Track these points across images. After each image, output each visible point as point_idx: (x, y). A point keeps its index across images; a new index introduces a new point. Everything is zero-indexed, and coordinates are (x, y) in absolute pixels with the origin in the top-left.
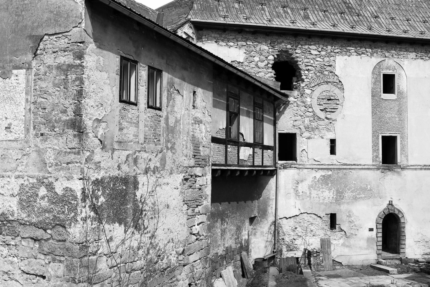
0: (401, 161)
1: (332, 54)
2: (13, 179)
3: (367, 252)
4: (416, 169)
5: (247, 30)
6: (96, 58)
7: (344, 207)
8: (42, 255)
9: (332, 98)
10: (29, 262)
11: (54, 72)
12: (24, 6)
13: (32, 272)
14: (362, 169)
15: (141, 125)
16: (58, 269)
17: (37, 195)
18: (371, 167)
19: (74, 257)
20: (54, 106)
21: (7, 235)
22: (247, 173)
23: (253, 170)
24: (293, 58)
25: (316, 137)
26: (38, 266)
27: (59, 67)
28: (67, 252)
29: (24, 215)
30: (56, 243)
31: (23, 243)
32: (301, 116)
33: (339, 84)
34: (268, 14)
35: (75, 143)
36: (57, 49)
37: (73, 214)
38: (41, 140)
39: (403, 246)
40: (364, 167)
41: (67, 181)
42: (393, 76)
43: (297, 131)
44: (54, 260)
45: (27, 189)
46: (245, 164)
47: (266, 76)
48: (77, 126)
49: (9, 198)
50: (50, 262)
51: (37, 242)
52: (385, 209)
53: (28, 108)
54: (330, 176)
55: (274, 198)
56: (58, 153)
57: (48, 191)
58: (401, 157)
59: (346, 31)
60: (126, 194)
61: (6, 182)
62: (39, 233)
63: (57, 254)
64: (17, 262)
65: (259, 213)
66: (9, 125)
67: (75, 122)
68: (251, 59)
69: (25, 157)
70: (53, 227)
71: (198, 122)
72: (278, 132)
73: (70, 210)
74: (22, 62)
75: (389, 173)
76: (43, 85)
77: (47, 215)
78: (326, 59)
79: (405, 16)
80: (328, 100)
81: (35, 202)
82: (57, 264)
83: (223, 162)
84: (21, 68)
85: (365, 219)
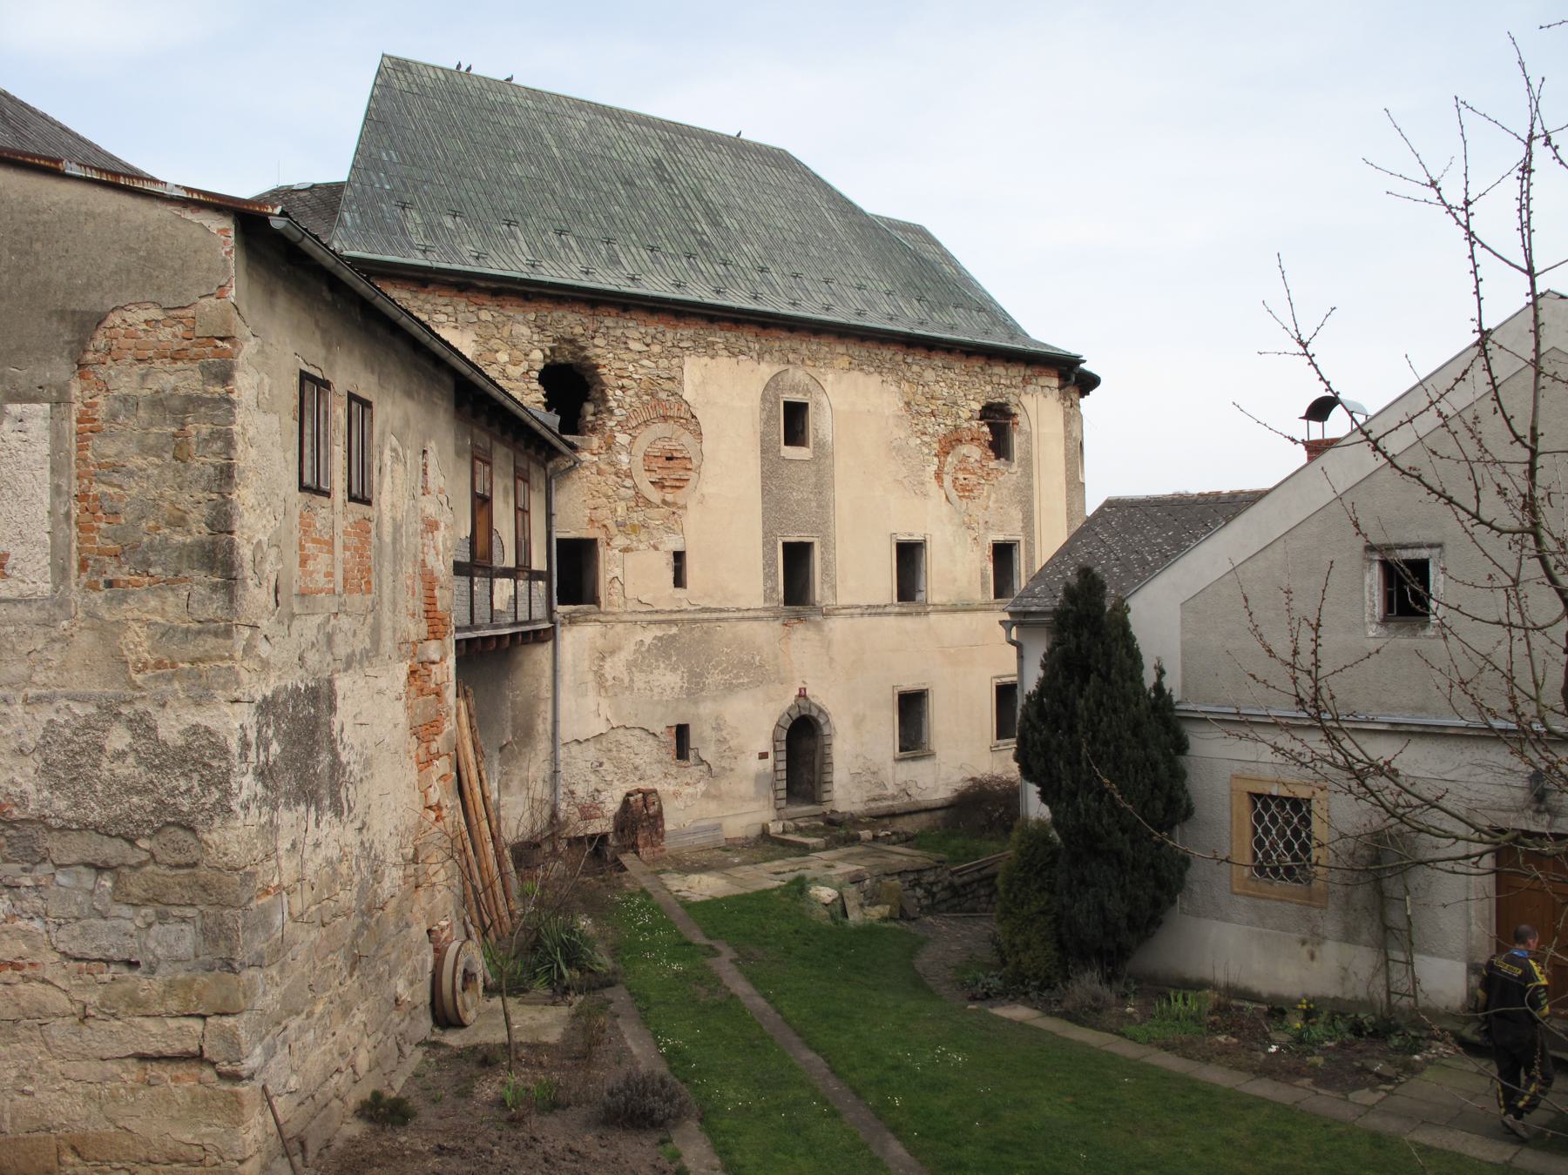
0: (823, 598)
1: (676, 350)
2: (19, 708)
3: (754, 806)
4: (852, 615)
5: (482, 284)
6: (257, 378)
7: (706, 709)
8: (125, 908)
11: (141, 413)
12: (41, 228)
13: (95, 955)
14: (743, 618)
15: (338, 544)
16: (178, 939)
17: (101, 749)
18: (762, 614)
19: (225, 907)
24: (587, 358)
25: (642, 546)
26: (113, 938)
27: (158, 402)
28: (203, 895)
29: (61, 804)
30: (168, 872)
31: (60, 878)
32: (608, 497)
33: (690, 422)
35: (214, 608)
36: (151, 353)
37: (217, 795)
39: (828, 787)
40: (746, 614)
42: (805, 406)
43: (599, 534)
44: (163, 918)
45: (67, 732)
47: (530, 397)
48: (218, 559)
50: (150, 925)
52: (791, 708)
53: (63, 510)
54: (674, 637)
55: (549, 695)
56: (163, 635)
57: (135, 736)
59: (707, 300)
60: (317, 726)
62: (112, 850)
63: (173, 900)
64: (42, 931)
69: (57, 646)
70: (157, 831)
71: (431, 526)
72: (556, 535)
73: (206, 784)
74: (39, 382)
75: (800, 626)
76: (110, 449)
77: (135, 800)
78: (663, 363)
79: (788, 264)
80: (668, 459)
81: (96, 766)
82: (174, 927)
84: (35, 400)
85: (749, 727)
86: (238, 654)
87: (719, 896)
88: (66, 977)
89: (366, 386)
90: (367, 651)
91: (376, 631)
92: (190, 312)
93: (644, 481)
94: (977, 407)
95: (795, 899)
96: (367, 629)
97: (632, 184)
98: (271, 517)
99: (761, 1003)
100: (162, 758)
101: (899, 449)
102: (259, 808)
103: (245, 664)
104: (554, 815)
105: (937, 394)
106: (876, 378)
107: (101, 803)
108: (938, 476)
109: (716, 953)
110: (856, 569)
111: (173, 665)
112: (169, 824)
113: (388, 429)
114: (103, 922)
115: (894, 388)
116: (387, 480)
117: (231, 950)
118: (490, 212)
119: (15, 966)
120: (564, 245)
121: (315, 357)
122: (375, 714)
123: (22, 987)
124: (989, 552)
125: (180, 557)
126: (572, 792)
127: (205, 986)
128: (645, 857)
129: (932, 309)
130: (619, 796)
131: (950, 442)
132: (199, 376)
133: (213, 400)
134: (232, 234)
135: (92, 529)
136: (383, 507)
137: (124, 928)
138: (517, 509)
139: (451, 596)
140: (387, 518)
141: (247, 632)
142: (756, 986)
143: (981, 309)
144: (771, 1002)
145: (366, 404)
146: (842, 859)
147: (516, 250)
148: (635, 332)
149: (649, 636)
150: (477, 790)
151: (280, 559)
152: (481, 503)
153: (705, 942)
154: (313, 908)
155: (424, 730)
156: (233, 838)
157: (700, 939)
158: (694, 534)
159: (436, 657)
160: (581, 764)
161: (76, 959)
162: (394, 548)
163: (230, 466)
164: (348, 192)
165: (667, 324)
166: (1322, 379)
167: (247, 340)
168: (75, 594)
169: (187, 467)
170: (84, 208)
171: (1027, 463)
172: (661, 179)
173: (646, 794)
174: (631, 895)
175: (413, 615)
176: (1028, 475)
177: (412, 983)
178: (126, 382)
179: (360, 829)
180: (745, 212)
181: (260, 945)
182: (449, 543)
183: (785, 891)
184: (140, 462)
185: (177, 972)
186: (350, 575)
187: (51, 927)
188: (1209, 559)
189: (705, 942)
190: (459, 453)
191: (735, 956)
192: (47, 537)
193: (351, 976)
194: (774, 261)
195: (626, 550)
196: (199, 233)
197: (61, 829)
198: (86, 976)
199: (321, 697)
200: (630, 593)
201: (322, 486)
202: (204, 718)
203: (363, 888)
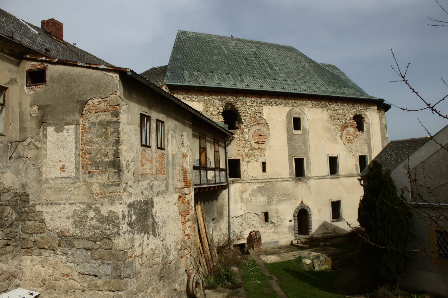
0: (307, 174)
1: (261, 105)
2: (68, 206)
3: (289, 235)
4: (316, 179)
7: (273, 207)
8: (94, 260)
9: (262, 134)
10: (84, 266)
11: (97, 126)
13: (87, 273)
15: (154, 161)
16: (107, 269)
17: (87, 217)
18: (289, 179)
19: (119, 261)
20: (98, 152)
21: (65, 247)
22: (212, 189)
23: (215, 186)
24: (236, 108)
25: (253, 161)
26: (91, 269)
27: (100, 123)
29: (78, 232)
31: (78, 252)
32: (243, 147)
33: (266, 125)
34: (217, 79)
35: (115, 179)
36: (99, 110)
37: (116, 230)
38: (89, 177)
40: (284, 180)
41: (110, 206)
42: (299, 119)
44: (103, 263)
45: (79, 213)
46: (211, 183)
47: (219, 120)
48: (116, 165)
49: (65, 220)
50: (100, 265)
51: (89, 251)
52: (299, 207)
53: (78, 153)
54: (263, 187)
55: (227, 204)
57: (96, 214)
58: (307, 171)
60: (147, 211)
61: (62, 208)
62: (90, 244)
64: (74, 266)
65: (217, 215)
66: (63, 166)
67: (115, 163)
68: (208, 109)
69: (77, 189)
70: (101, 240)
71: (185, 156)
72: (228, 158)
73: (113, 227)
74: (72, 120)
77: (96, 231)
78: (257, 108)
79: (293, 78)
80: (260, 136)
81: (86, 222)
82: (106, 266)
83: (199, 183)
84: (71, 124)
85: (286, 213)
86: (122, 191)
87: (276, 262)
88: (79, 279)
89: (162, 117)
90: (164, 191)
91: (167, 186)
92: (108, 99)
93: (253, 142)
94: (352, 116)
95: (298, 263)
96: (164, 185)
97: (248, 59)
98: (132, 153)
99: (283, 293)
100: (103, 220)
101: (328, 130)
102: (129, 234)
103: (124, 194)
104: (229, 238)
105: (339, 113)
106: (321, 109)
107: (87, 232)
108: (341, 137)
109: (272, 278)
110: (317, 166)
111: (105, 194)
112: (104, 238)
113: (170, 129)
114: (88, 264)
115: (326, 112)
116: (170, 143)
117: (121, 273)
118: (207, 70)
119: (68, 276)
120: (228, 77)
121: (146, 111)
122: (167, 209)
123: (69, 281)
124: (358, 159)
125: (106, 165)
126: (234, 232)
127: (114, 283)
128: (256, 251)
129: (337, 88)
130: (248, 233)
131: (345, 127)
132: (111, 116)
133: (114, 122)
134: (118, 77)
135: (85, 158)
136: (169, 150)
137: (93, 266)
138: (215, 151)
139: (193, 176)
140: (170, 153)
141: (124, 185)
142: (282, 288)
143: (352, 88)
144: (286, 293)
145: (163, 122)
146: (314, 251)
147: (214, 80)
148: (248, 100)
149: (256, 186)
150: (204, 231)
151: (135, 165)
152: (203, 150)
153: (269, 275)
154: (147, 262)
155: (184, 213)
156: (120, 242)
157: (268, 274)
158: (268, 157)
159: (188, 193)
160: (237, 224)
161: (82, 274)
162: (173, 162)
163: (119, 140)
164: (168, 67)
165: (258, 97)
166: (411, 88)
167: (123, 105)
168: (81, 176)
169: (108, 140)
170: (83, 74)
171: (368, 132)
172: (256, 57)
173: (256, 232)
174: (250, 261)
175: (180, 181)
176: (369, 135)
177: (180, 285)
178: (93, 118)
179: (162, 241)
180: (281, 65)
181: (129, 272)
182: (191, 161)
183: (295, 260)
184: (96, 139)
185: (107, 279)
186: (158, 169)
187: (76, 265)
188: (417, 157)
189: (269, 275)
190: (194, 136)
191: (277, 279)
192: (74, 160)
193: (160, 282)
194: (289, 78)
195: (248, 162)
196: (110, 78)
197: (78, 239)
198: (84, 279)
199: (149, 203)
200: (250, 175)
201: (148, 144)
202: (113, 208)
203: (164, 258)
